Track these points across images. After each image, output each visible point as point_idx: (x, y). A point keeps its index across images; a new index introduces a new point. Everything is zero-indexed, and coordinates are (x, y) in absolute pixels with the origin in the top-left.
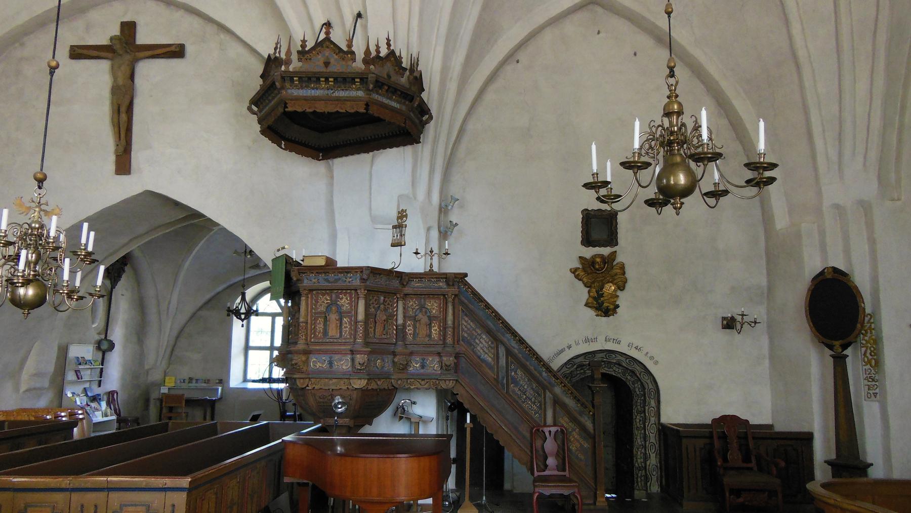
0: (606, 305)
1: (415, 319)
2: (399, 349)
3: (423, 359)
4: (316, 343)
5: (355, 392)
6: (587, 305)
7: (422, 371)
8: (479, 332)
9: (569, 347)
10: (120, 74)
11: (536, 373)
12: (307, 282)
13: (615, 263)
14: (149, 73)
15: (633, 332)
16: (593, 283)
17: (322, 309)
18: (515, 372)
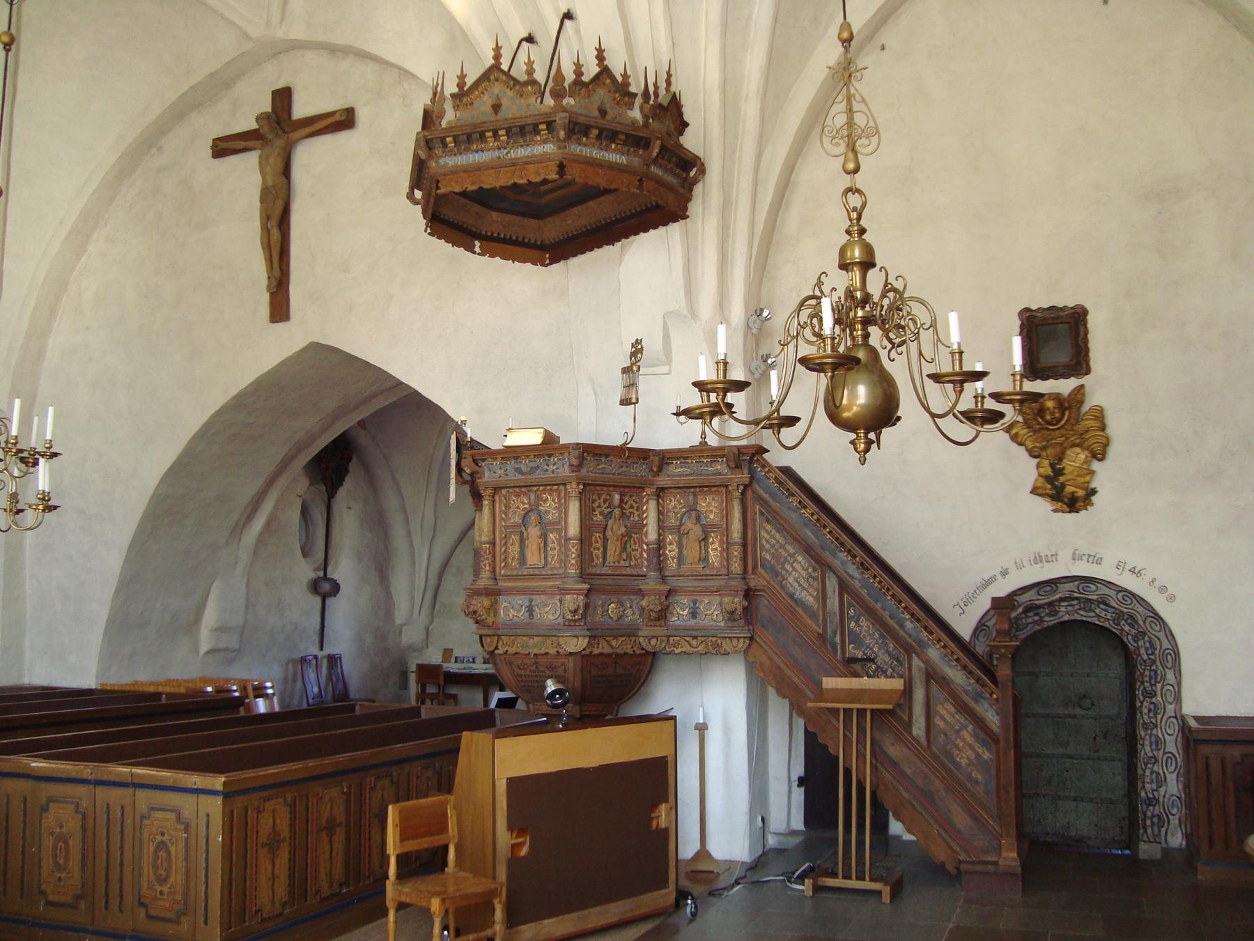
0: (1069, 489)
1: (679, 530)
3: (695, 602)
4: (509, 578)
5: (571, 659)
6: (1034, 491)
7: (693, 622)
8: (792, 551)
9: (1005, 573)
10: (268, 169)
11: (892, 622)
12: (491, 474)
13: (1085, 408)
14: (312, 158)
15: (1124, 542)
16: (1044, 448)
17: (517, 519)
18: (857, 622)
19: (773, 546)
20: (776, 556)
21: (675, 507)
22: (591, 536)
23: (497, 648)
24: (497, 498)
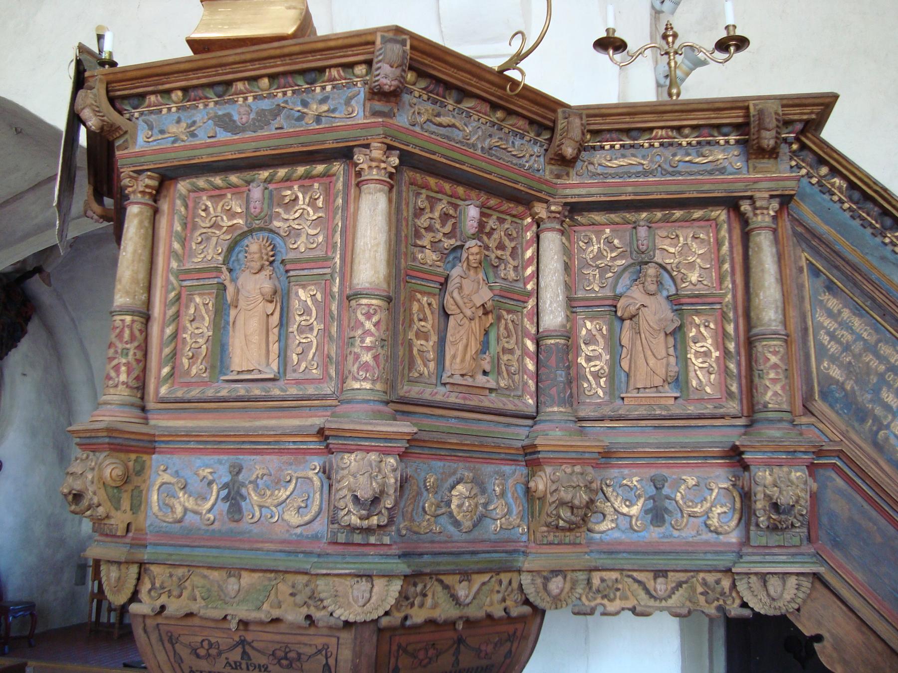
2: (552, 435)
3: (658, 483)
5: (346, 637)
7: (654, 534)
17: (210, 253)
19: (847, 348)
20: (860, 375)
21: (600, 255)
22: (412, 298)
23: (134, 597)
24: (165, 206)
